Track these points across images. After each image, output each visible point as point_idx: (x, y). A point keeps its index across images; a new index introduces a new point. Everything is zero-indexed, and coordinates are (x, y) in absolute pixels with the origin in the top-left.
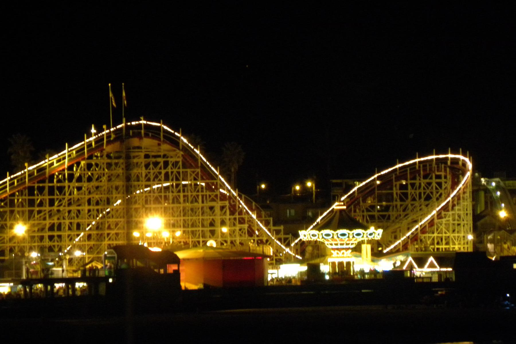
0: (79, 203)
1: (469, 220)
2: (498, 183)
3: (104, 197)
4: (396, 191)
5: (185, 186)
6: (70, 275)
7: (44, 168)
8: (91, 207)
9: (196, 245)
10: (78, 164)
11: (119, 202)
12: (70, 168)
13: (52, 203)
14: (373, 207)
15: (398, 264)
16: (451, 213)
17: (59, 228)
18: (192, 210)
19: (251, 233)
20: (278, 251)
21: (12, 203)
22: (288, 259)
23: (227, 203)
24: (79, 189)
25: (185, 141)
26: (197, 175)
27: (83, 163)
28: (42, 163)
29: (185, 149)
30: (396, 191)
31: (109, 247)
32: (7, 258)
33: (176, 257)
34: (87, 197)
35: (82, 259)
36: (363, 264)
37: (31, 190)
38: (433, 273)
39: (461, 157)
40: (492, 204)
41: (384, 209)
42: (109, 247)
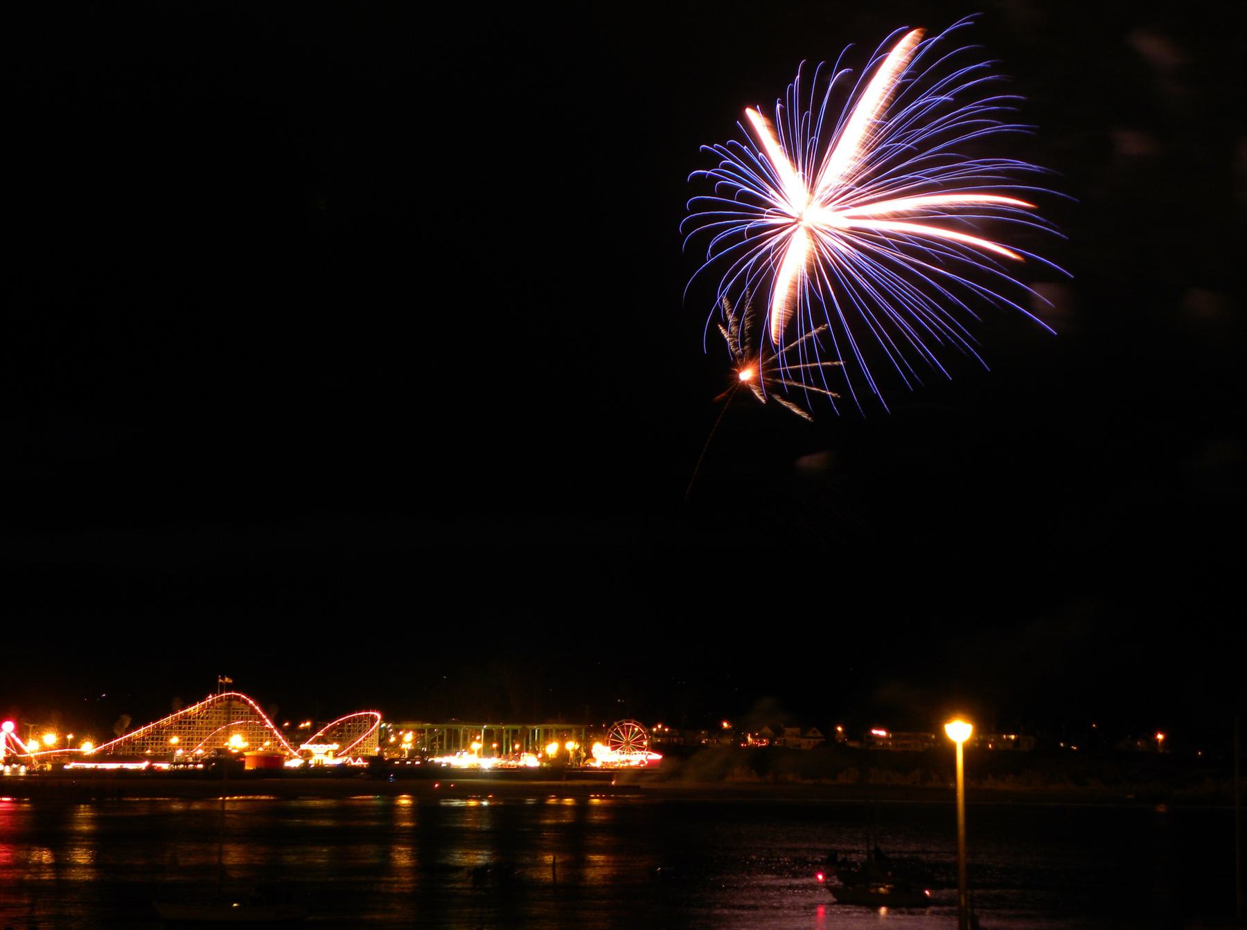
30: (346, 728)
36: (330, 761)
40: (387, 736)
41: (341, 736)
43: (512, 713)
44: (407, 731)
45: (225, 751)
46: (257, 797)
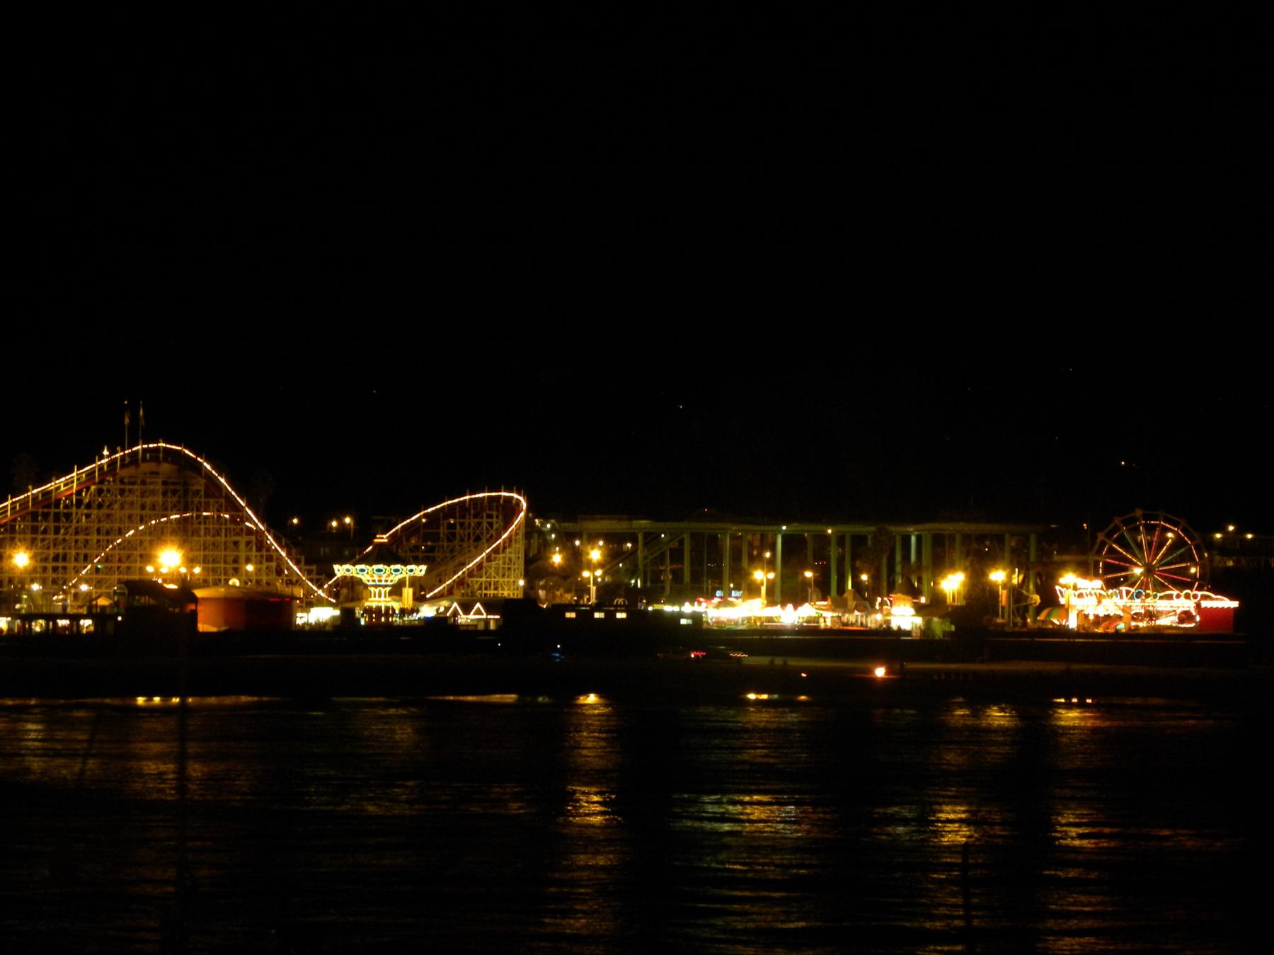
0: (87, 531)
1: (520, 565)
2: (553, 526)
3: (116, 526)
4: (443, 531)
5: (206, 517)
6: (75, 611)
7: (50, 492)
8: (101, 537)
9: (216, 583)
10: (88, 489)
11: (131, 532)
12: (79, 493)
13: (57, 531)
14: (417, 548)
15: (442, 609)
16: (501, 555)
17: (65, 558)
18: (214, 544)
19: (279, 572)
20: (309, 592)
21: (13, 530)
22: (320, 602)
23: (253, 538)
24: (88, 516)
25: (208, 467)
26: (221, 506)
27: (93, 488)
28: (50, 486)
29: (208, 476)
30: (443, 531)
31: (120, 582)
32: (5, 589)
33: (194, 595)
34: (96, 526)
35: (88, 594)
37: (34, 516)
38: (479, 620)
39: (515, 496)
40: (546, 546)
41: (436, 548)
42: (120, 582)
43: (850, 501)
44: (592, 538)
45: (149, 588)
46: (485, 698)
